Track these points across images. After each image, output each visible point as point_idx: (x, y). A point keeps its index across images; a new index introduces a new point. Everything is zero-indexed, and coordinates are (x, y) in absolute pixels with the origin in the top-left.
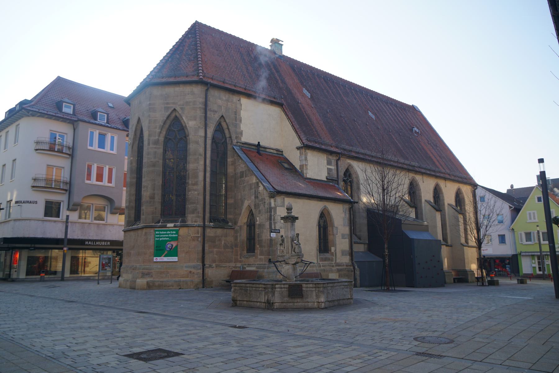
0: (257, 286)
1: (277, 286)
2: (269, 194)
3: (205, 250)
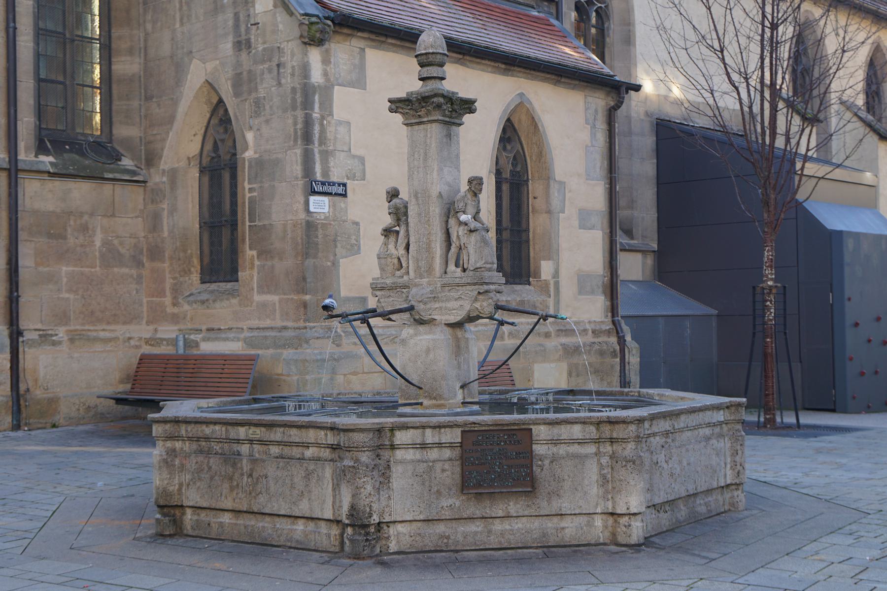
0: (295, 435)
1: (401, 437)
2: (302, 24)
3: (20, 269)
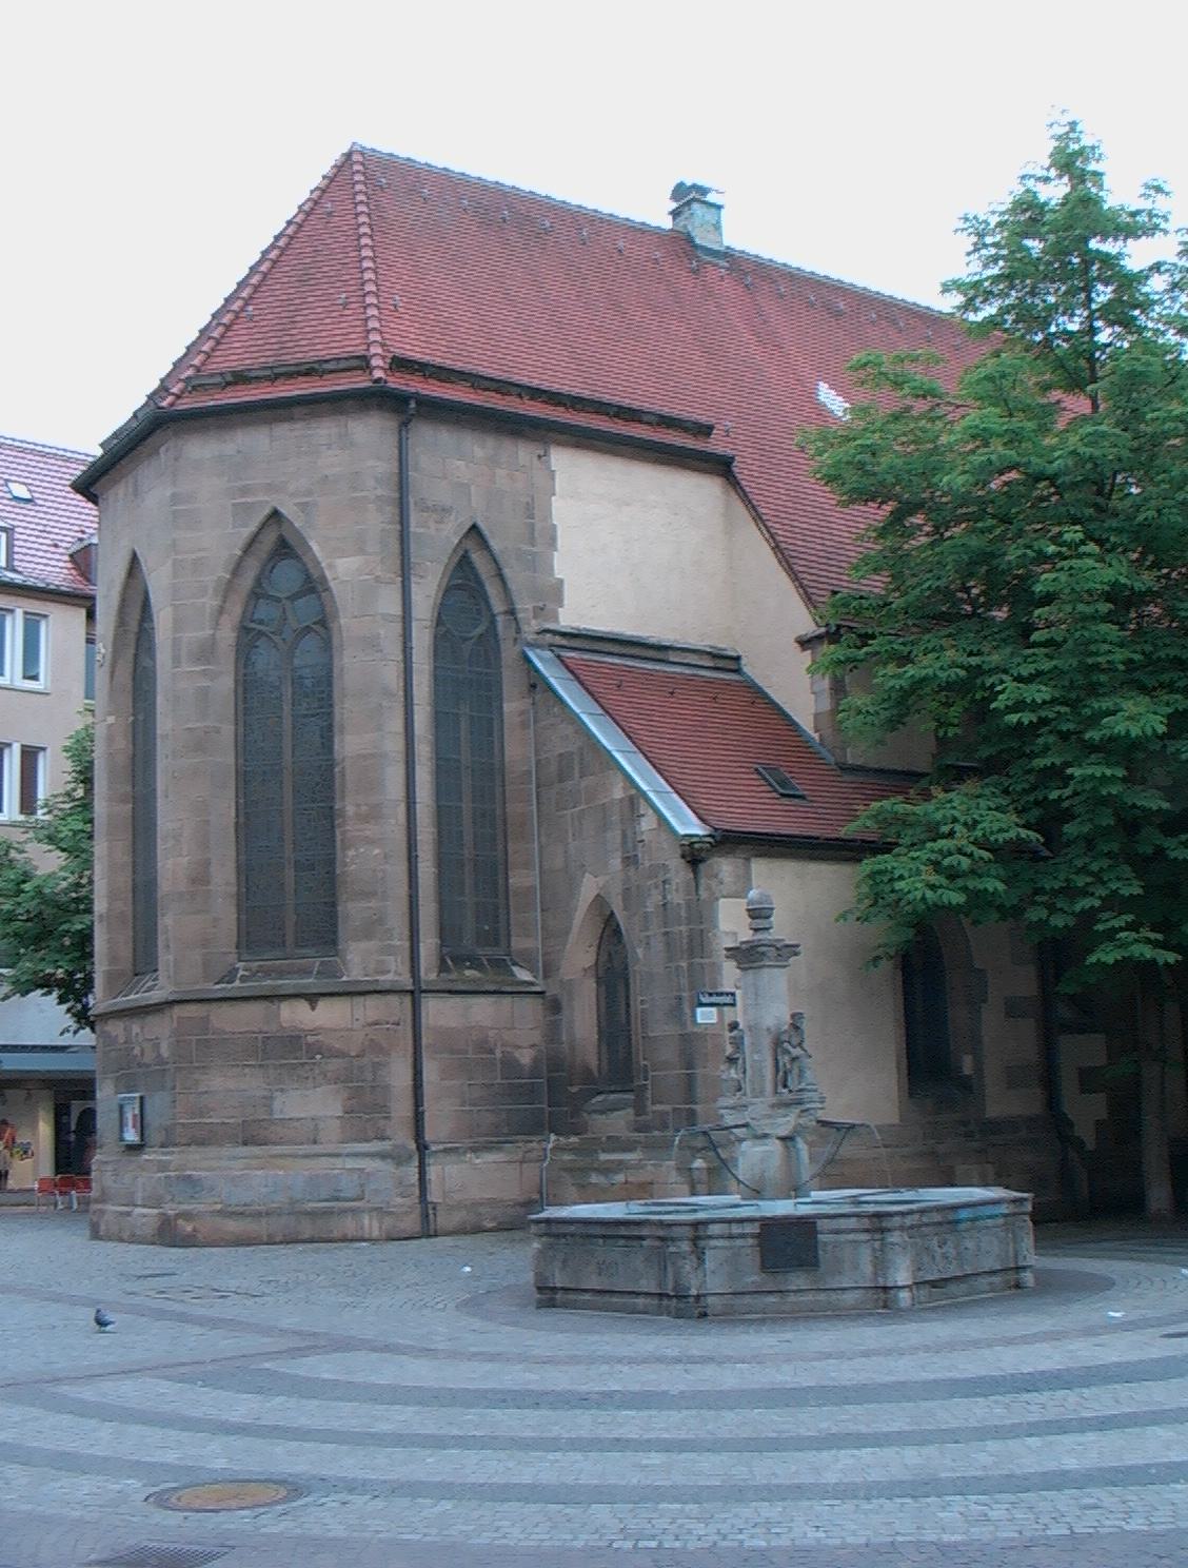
1: (715, 1229)
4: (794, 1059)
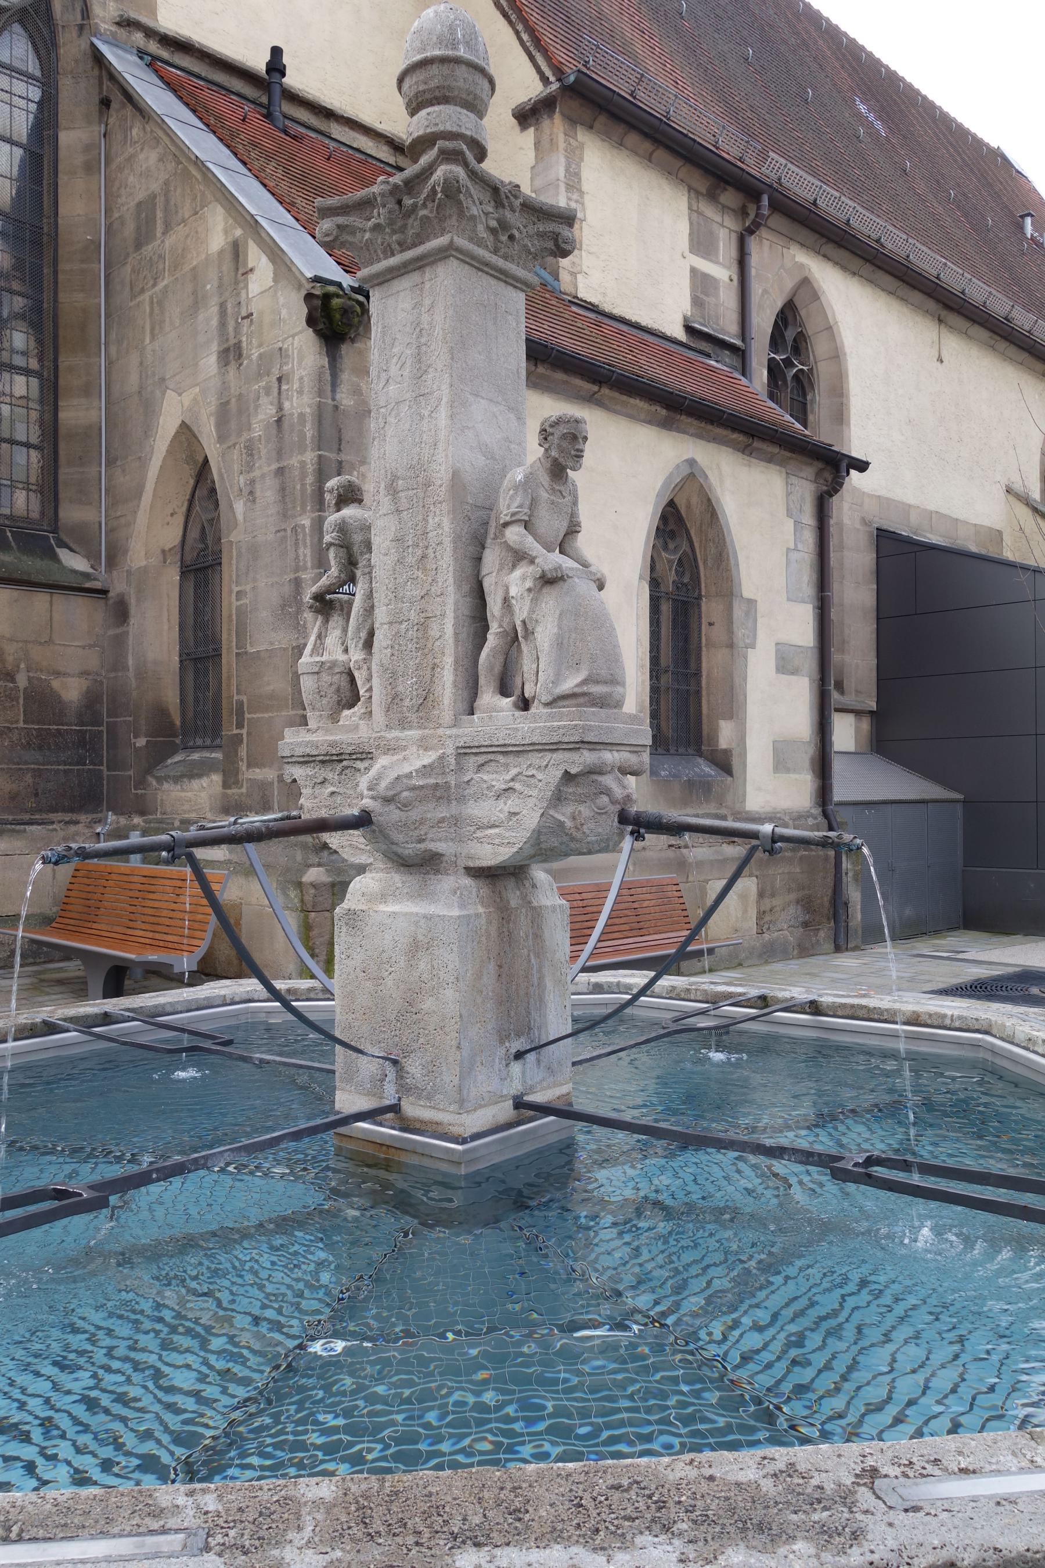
4: (549, 580)
